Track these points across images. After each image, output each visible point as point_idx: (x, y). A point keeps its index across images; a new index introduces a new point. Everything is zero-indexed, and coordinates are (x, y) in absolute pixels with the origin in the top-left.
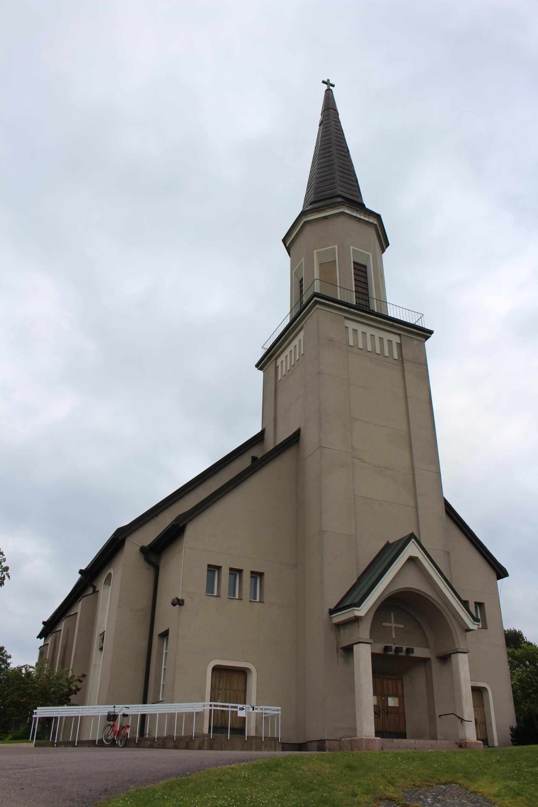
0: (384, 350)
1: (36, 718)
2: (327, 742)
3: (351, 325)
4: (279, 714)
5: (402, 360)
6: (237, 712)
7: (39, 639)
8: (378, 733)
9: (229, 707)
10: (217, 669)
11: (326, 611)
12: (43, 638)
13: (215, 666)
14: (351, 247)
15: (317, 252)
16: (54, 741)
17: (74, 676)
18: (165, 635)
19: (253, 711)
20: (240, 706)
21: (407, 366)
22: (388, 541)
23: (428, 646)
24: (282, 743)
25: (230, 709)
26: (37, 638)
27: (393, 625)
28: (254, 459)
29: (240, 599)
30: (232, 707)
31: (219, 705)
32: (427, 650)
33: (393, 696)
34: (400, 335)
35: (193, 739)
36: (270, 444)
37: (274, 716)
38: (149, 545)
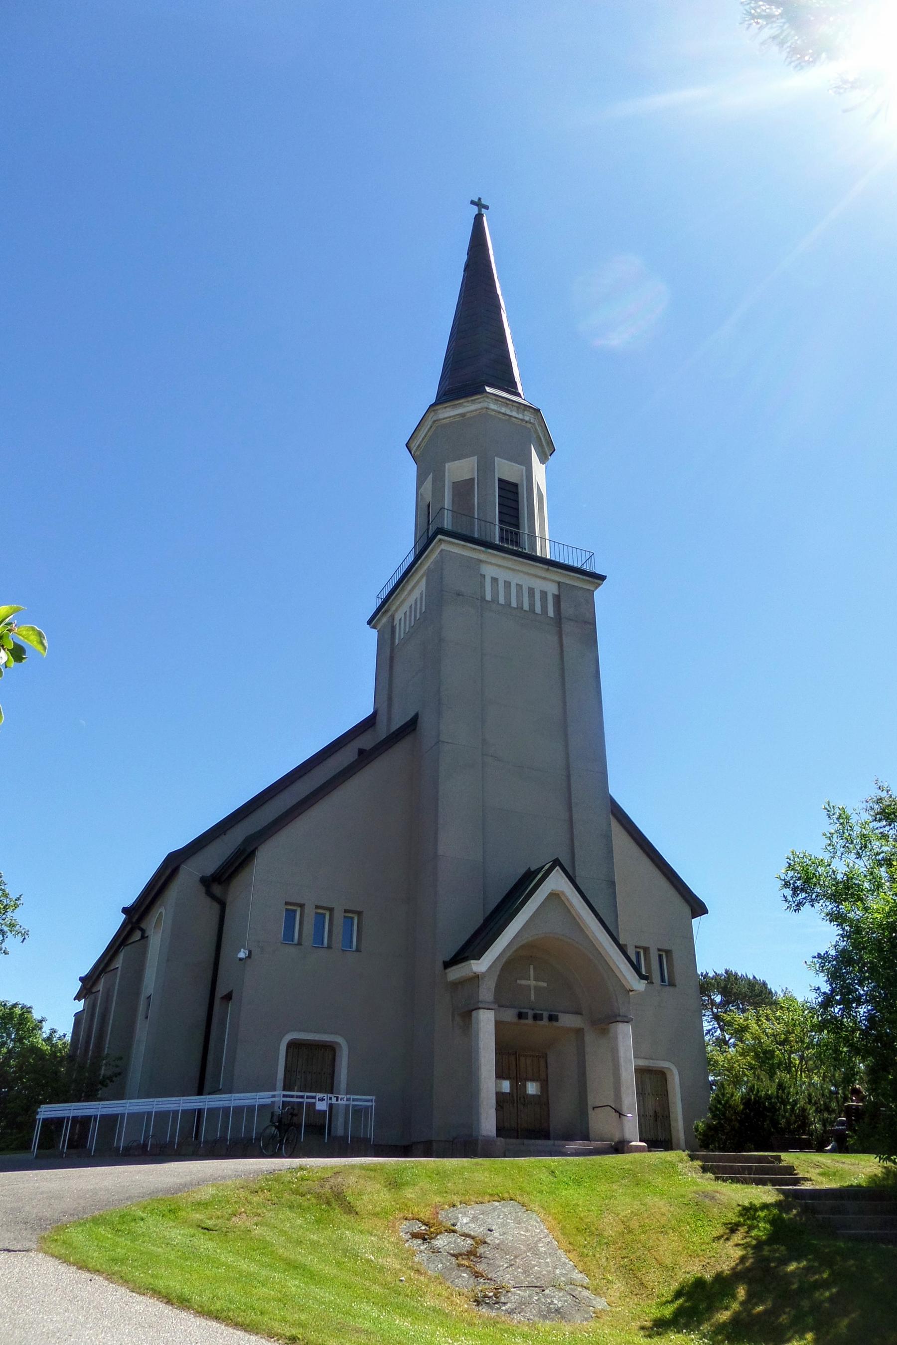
0: (534, 604)
1: (40, 1119)
2: (434, 1144)
4: (372, 1106)
5: (560, 619)
6: (314, 1104)
7: (77, 1001)
8: (500, 1131)
10: (295, 1046)
11: (439, 965)
12: (83, 1000)
13: (287, 1044)
17: (109, 1054)
18: (228, 997)
19: (337, 1102)
20: (319, 1095)
21: (567, 627)
22: (529, 868)
24: (376, 1145)
25: (306, 1100)
26: (75, 1000)
27: (532, 983)
28: (361, 752)
29: (329, 947)
30: (308, 1097)
31: (296, 1096)
33: (532, 1080)
35: (253, 1142)
36: (382, 731)
37: (367, 1108)
38: (212, 875)
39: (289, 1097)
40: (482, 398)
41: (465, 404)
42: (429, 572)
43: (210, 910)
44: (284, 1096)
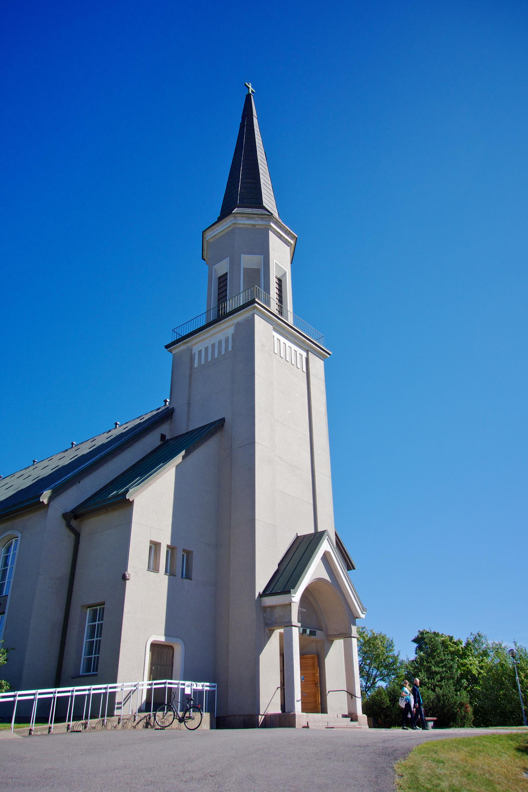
25: (168, 686)
40: (268, 218)
41: (257, 219)
42: (238, 325)
43: (68, 539)
44: (115, 687)
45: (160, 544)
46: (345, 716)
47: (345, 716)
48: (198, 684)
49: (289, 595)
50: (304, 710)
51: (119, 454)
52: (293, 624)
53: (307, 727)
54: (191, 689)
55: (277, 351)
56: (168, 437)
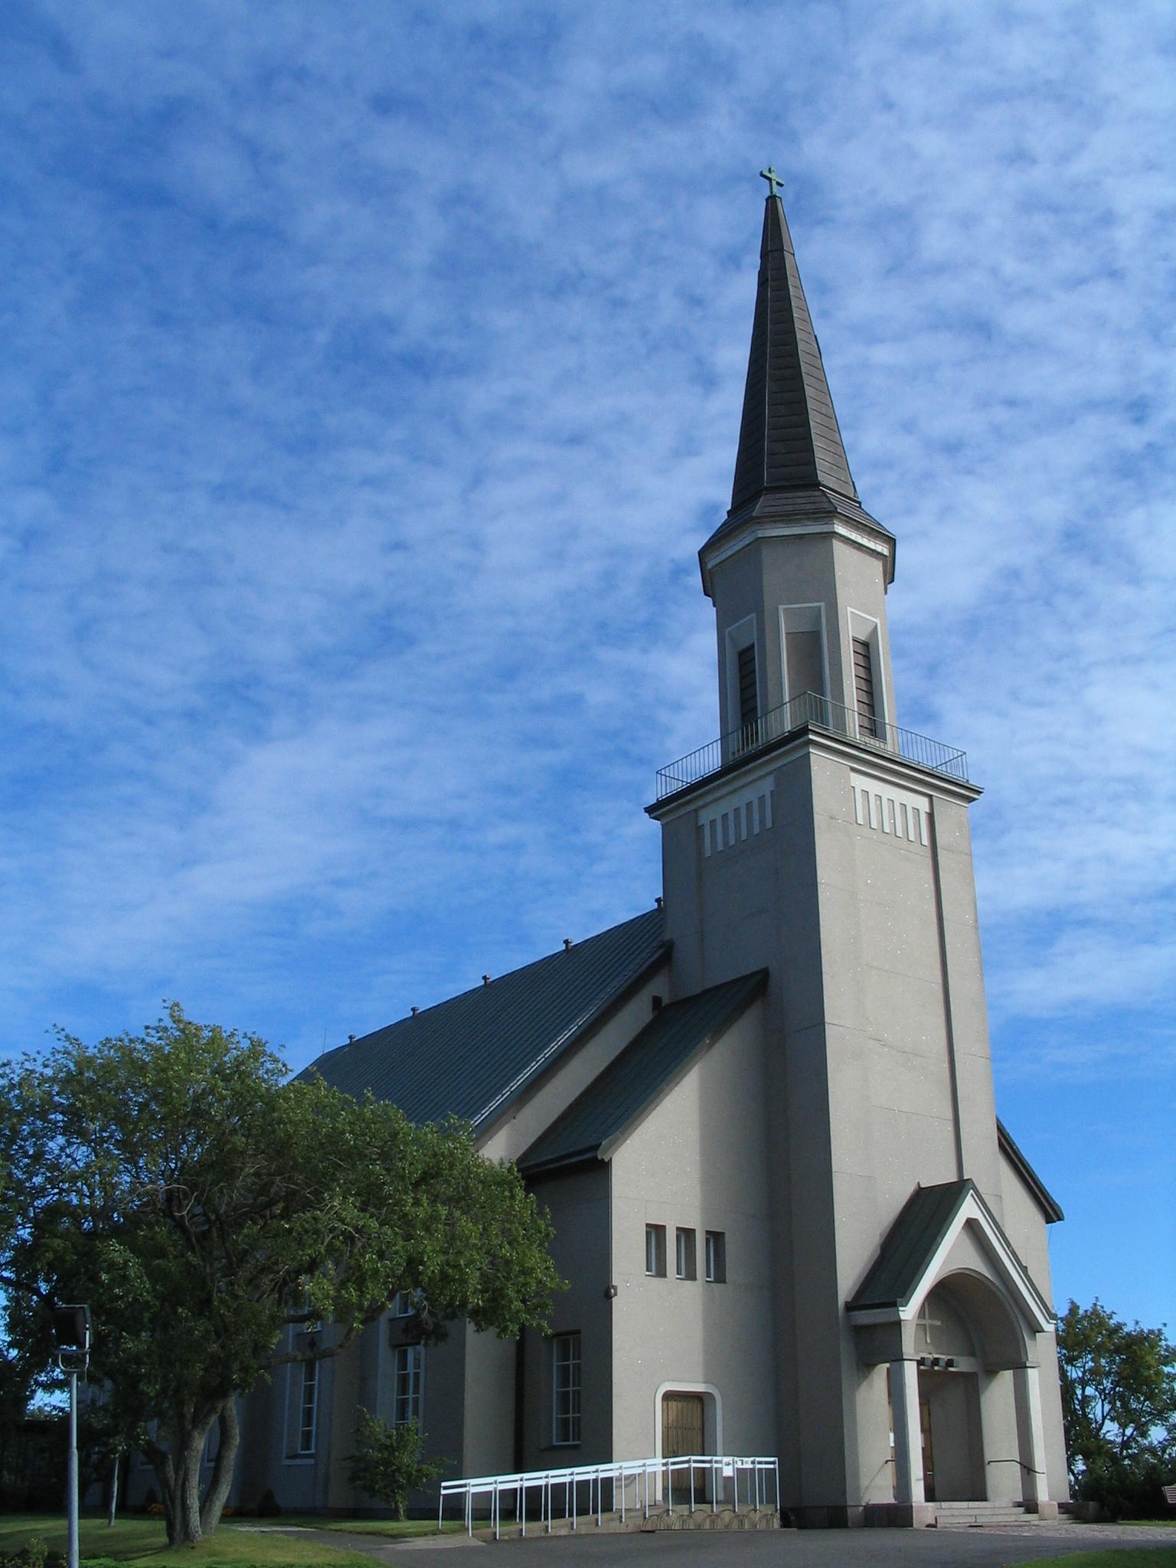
3: (859, 782)
6: (721, 1469)
9: (694, 1462)
10: (669, 1396)
13: (666, 1392)
14: (849, 609)
15: (785, 609)
16: (462, 1522)
23: (973, 1354)
32: (972, 1360)
34: (930, 797)
39: (418, 1381)
45: (664, 1227)
46: (1019, 1505)
47: (1019, 1505)
48: (745, 1459)
49: (894, 1309)
50: (930, 1496)
51: (580, 1050)
52: (905, 1357)
53: (934, 1526)
54: (734, 1469)
55: (862, 820)
56: (666, 1001)
